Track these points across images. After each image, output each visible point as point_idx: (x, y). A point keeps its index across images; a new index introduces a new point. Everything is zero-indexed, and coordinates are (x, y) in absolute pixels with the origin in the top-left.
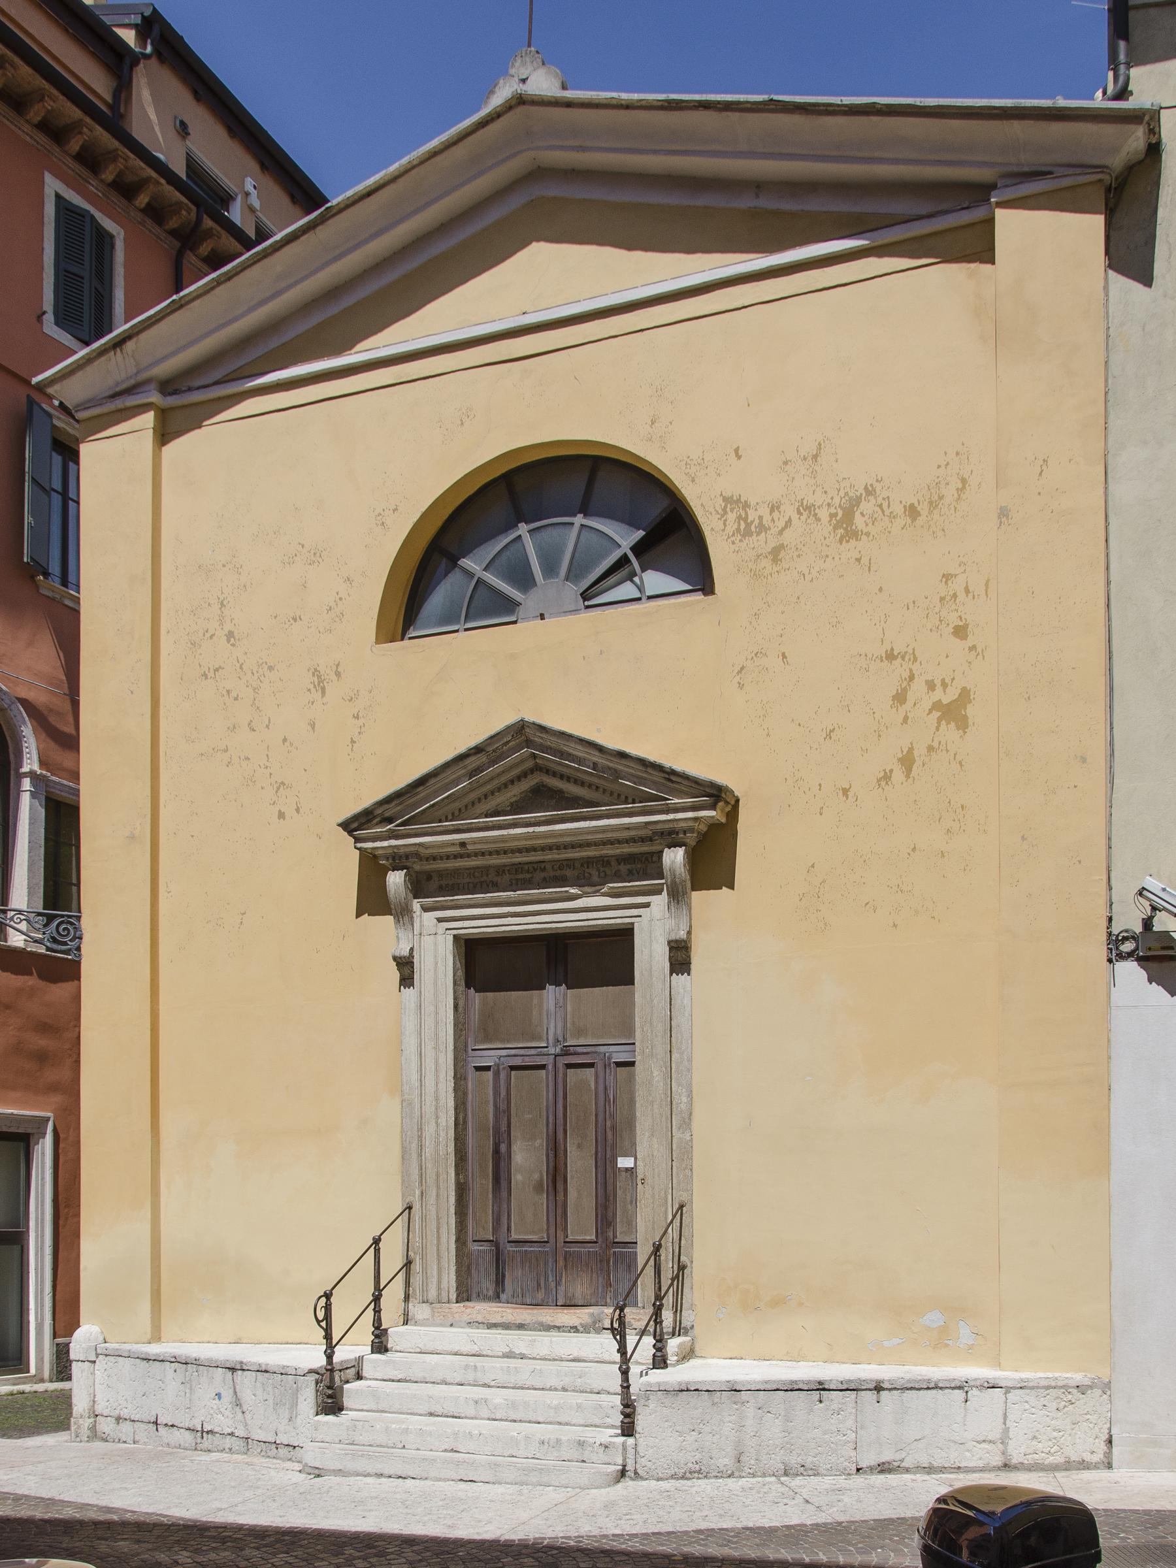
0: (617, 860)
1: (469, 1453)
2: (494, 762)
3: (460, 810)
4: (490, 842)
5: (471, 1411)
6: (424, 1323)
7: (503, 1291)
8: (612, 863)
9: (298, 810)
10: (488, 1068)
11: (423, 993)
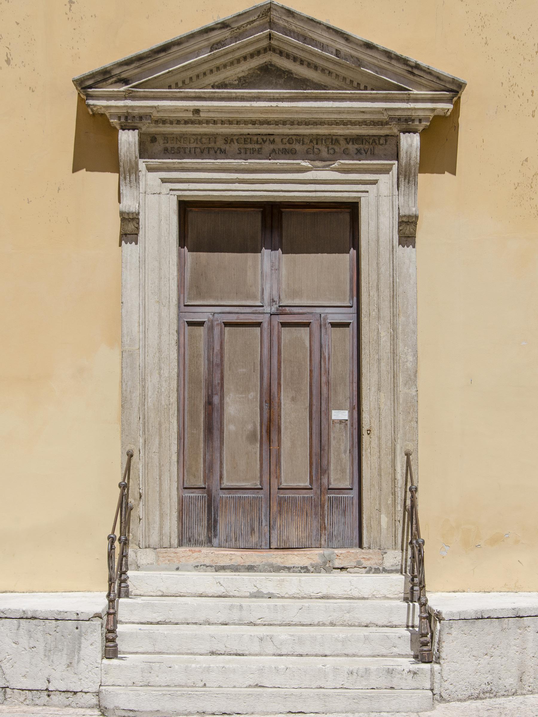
0: (346, 139)
1: (275, 687)
2: (236, 38)
3: (191, 79)
4: (224, 112)
5: (256, 649)
6: (149, 567)
7: (215, 536)
8: (341, 142)
9: (8, 61)
10: (201, 324)
11: (147, 249)
